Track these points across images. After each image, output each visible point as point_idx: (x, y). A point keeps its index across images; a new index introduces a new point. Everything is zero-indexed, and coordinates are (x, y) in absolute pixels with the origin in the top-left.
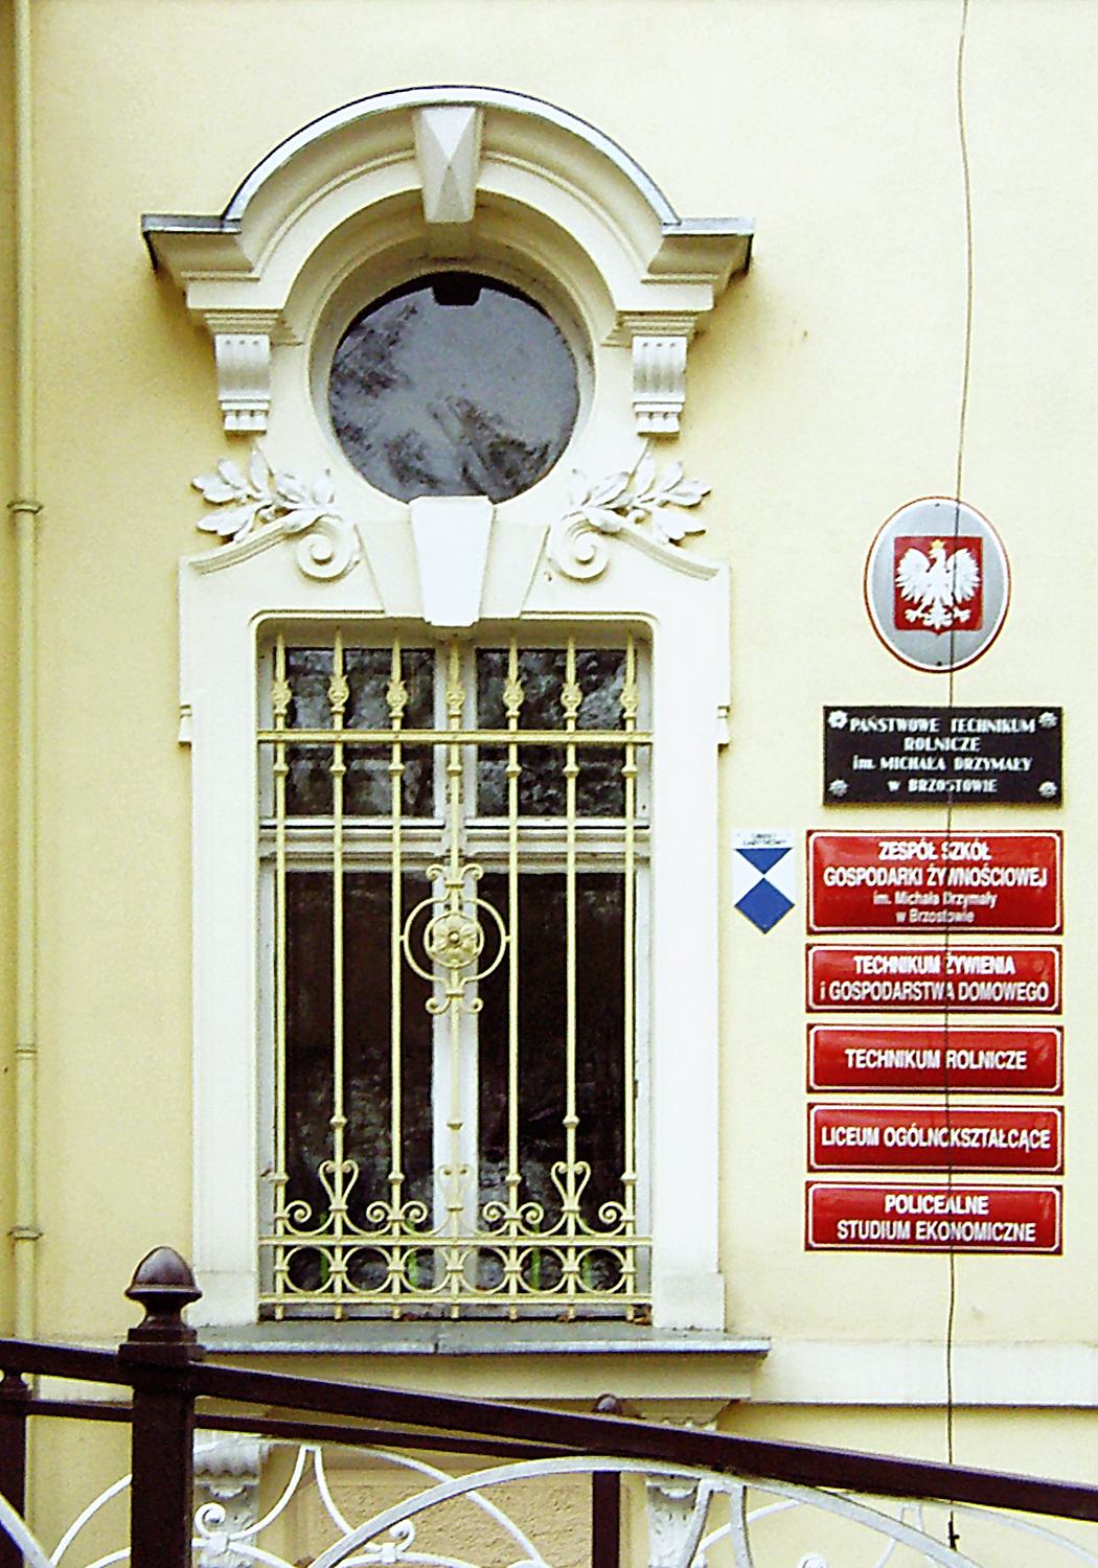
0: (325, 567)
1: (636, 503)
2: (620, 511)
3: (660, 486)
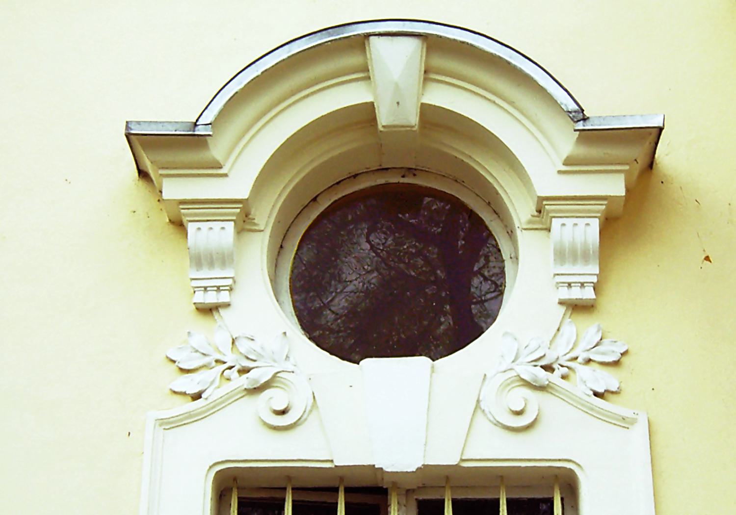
2: (548, 368)
3: (583, 345)
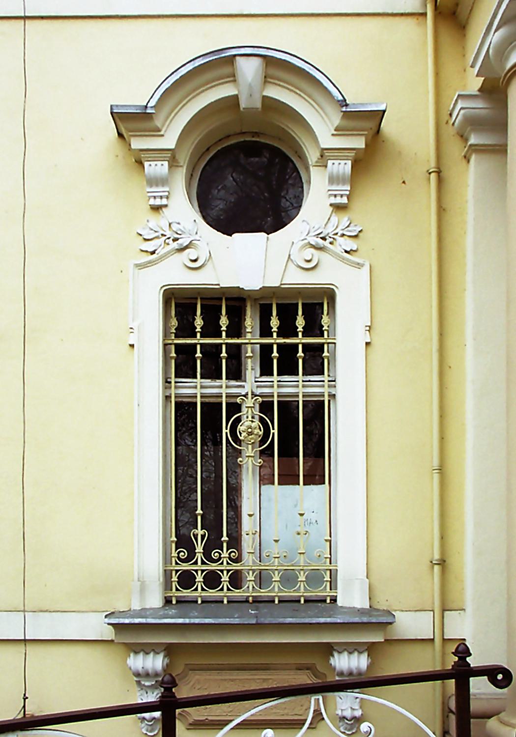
0: (196, 263)
1: (331, 235)
2: (324, 239)
